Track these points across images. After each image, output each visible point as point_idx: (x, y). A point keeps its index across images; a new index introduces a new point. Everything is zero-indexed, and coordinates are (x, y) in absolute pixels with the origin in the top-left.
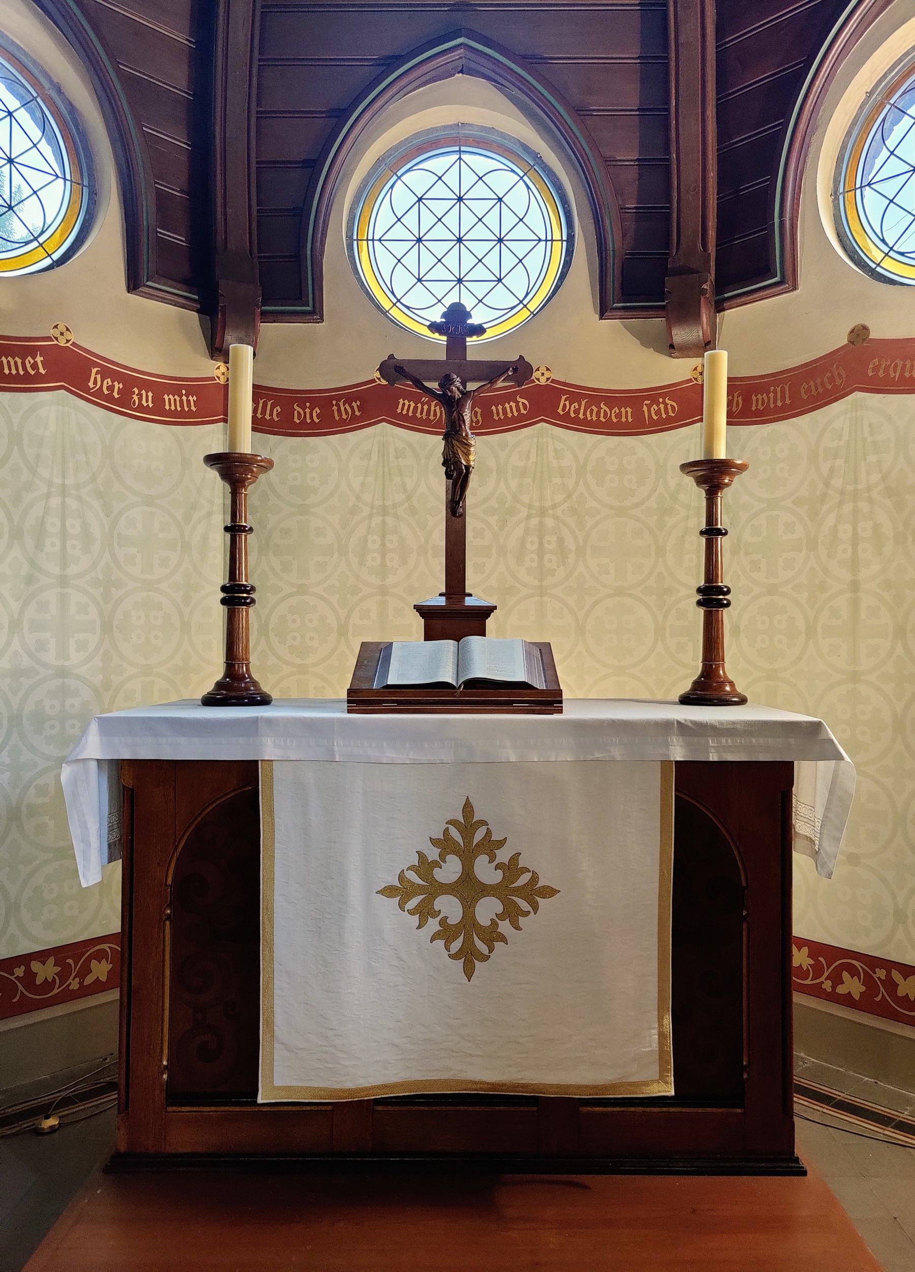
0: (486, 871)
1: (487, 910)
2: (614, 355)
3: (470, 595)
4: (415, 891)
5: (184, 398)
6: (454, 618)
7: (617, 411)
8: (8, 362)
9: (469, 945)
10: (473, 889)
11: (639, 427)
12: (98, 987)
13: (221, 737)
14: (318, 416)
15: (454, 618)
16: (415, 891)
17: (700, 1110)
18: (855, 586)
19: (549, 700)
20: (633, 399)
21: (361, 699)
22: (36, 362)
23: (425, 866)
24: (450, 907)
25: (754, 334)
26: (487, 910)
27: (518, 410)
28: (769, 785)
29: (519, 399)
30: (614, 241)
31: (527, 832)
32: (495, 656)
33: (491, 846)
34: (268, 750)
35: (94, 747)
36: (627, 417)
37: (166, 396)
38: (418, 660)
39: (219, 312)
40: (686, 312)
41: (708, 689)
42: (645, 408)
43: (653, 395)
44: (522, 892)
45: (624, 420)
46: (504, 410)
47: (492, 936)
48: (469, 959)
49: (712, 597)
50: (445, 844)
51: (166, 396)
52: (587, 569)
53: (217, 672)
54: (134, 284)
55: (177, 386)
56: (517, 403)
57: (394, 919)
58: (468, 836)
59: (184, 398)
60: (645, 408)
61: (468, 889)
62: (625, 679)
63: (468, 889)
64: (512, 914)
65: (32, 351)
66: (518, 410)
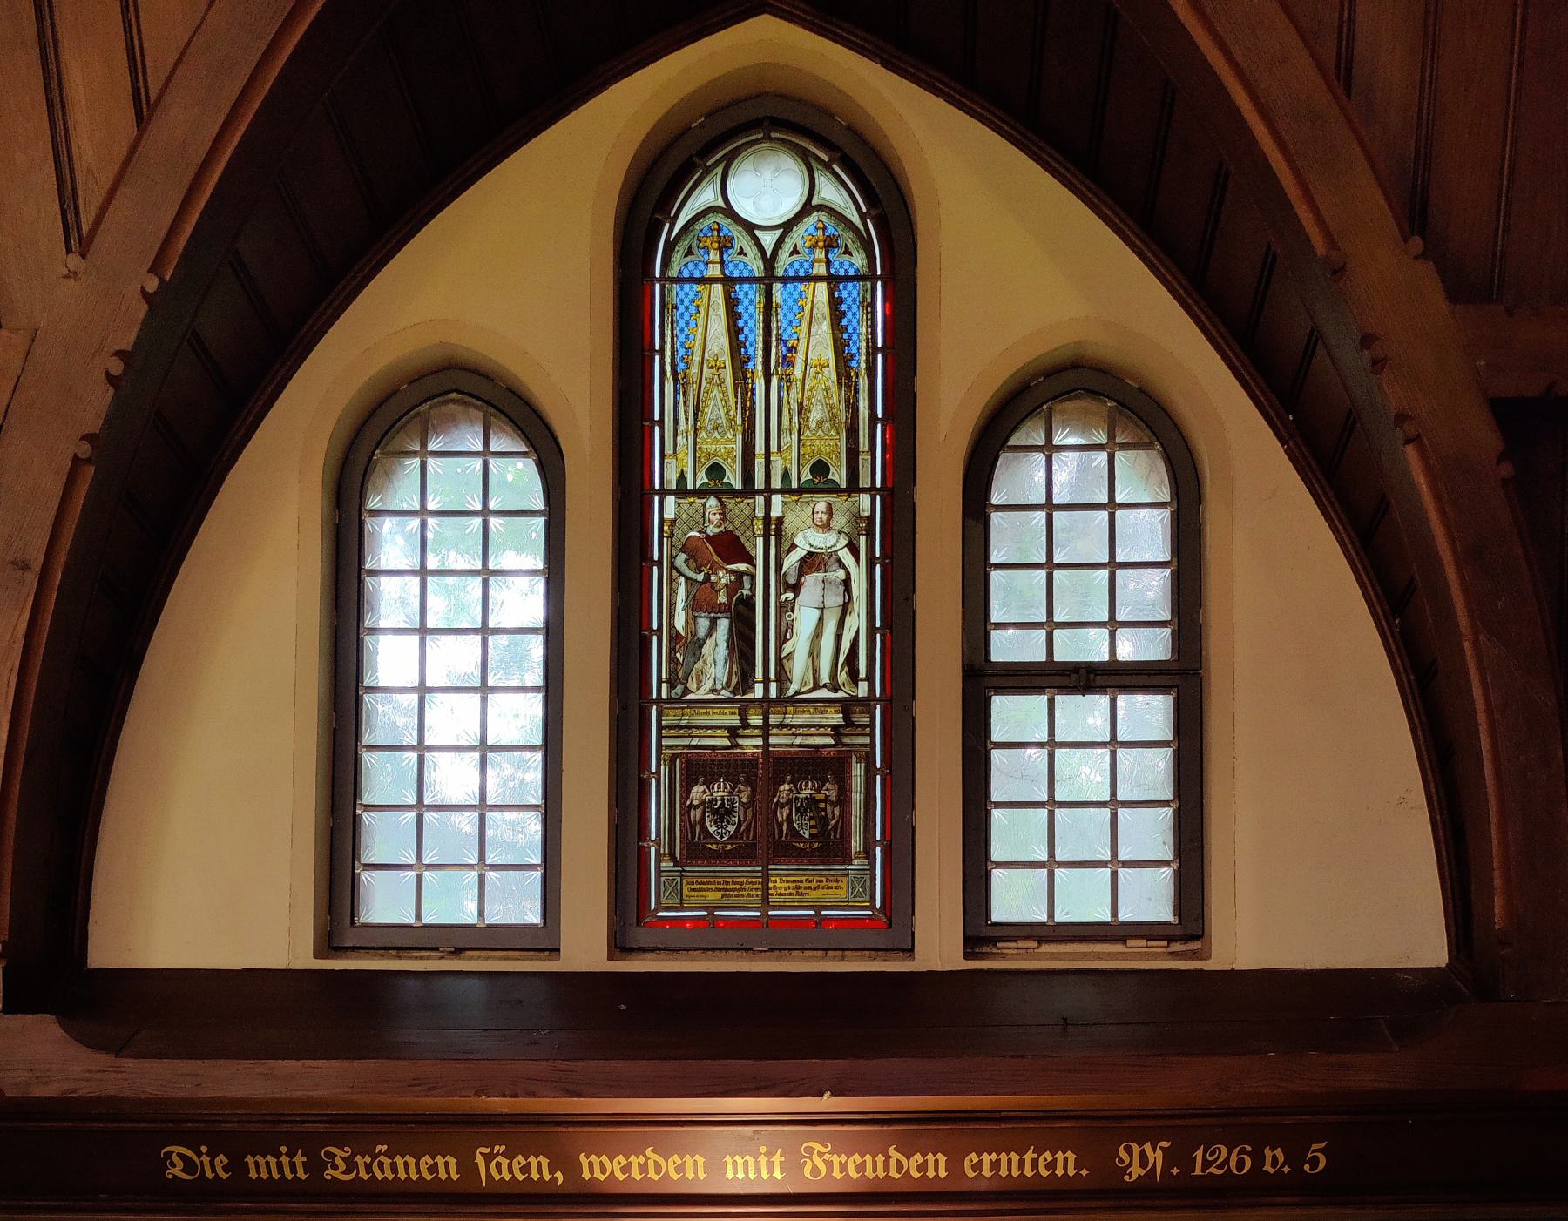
5: (285, 1160)
7: (1050, 1159)
8: (257, 1163)
14: (225, 1169)
17: (1451, 575)
19: (638, 924)
21: (890, 926)
22: (436, 1164)
27: (887, 1168)
29: (891, 1151)
36: (1065, 1168)
37: (249, 1159)
39: (820, 461)
42: (480, 1160)
45: (1060, 1172)
46: (758, 1170)
51: (249, 1159)
56: (888, 1158)
59: (285, 1160)
60: (480, 1160)
66: (887, 1168)
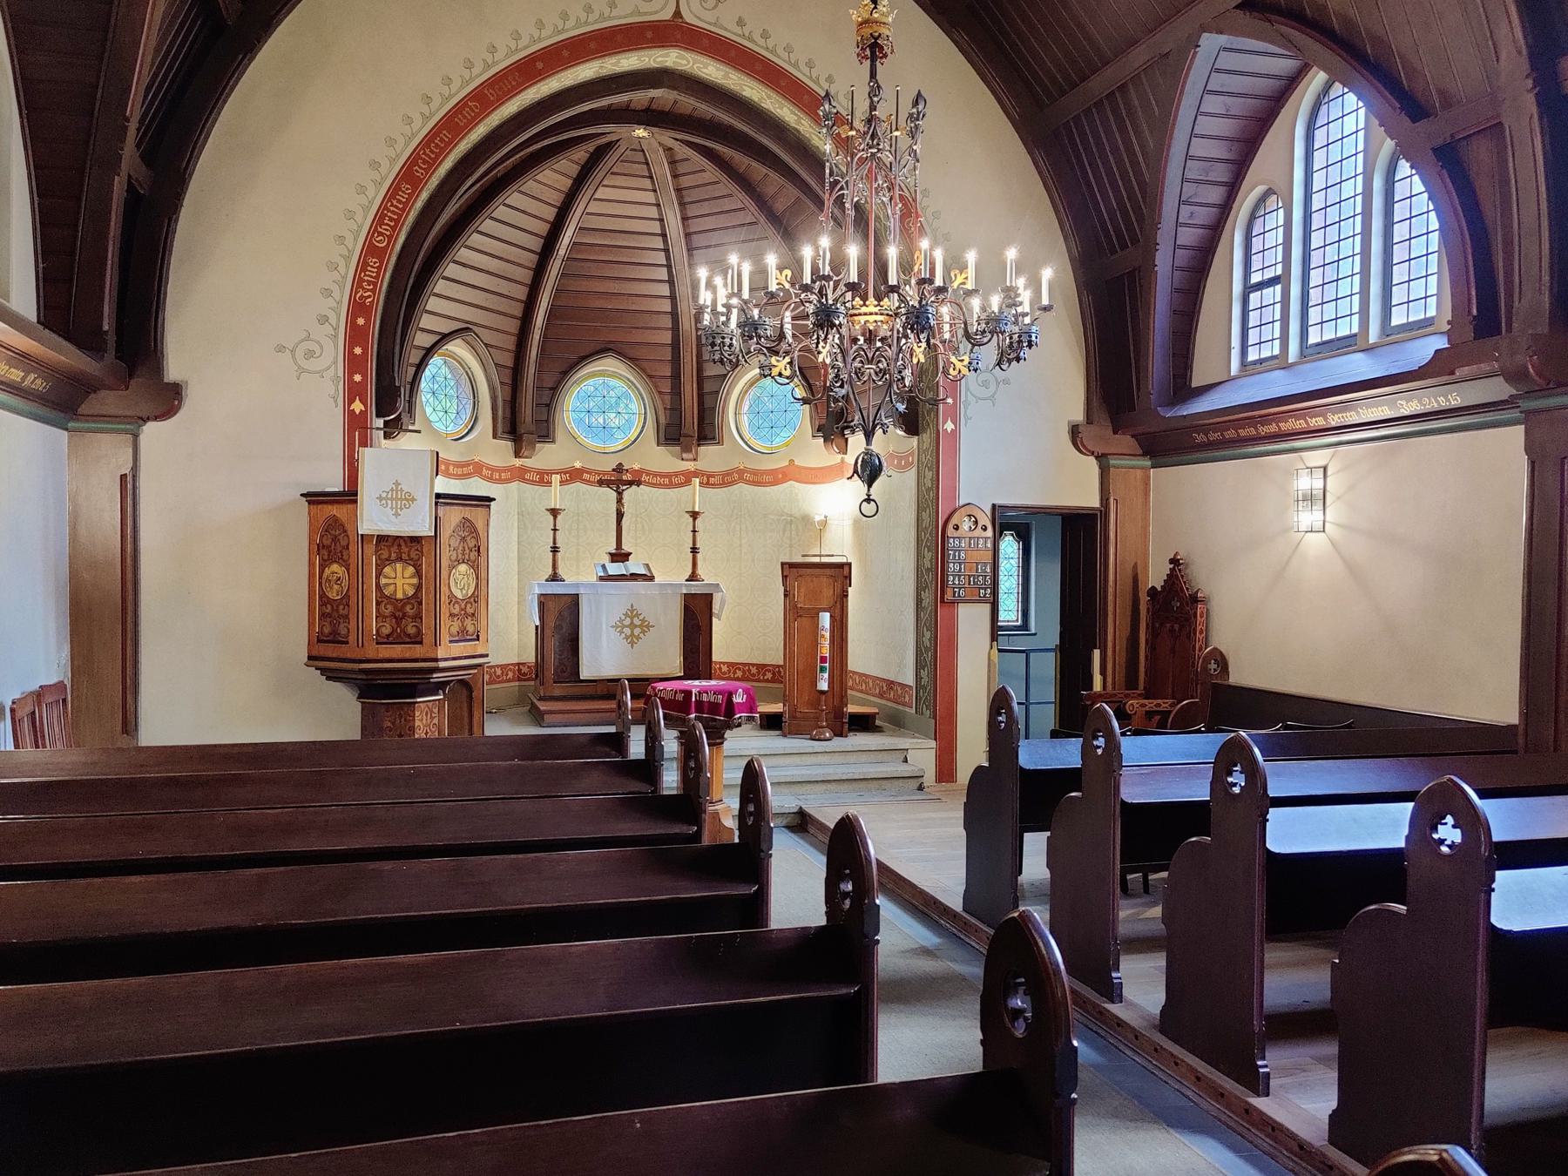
0: (637, 622)
1: (637, 631)
2: (665, 460)
3: (697, 614)
4: (619, 627)
6: (620, 556)
9: (632, 640)
10: (635, 627)
11: (671, 486)
12: (509, 681)
13: (695, 588)
15: (620, 556)
16: (619, 627)
19: (652, 578)
20: (668, 475)
23: (621, 621)
24: (627, 631)
25: (710, 457)
26: (637, 631)
28: (707, 599)
30: (663, 420)
31: (648, 612)
32: (634, 566)
33: (638, 615)
34: (581, 591)
35: (537, 591)
38: (615, 569)
40: (687, 449)
41: (693, 577)
43: (676, 474)
44: (646, 627)
47: (638, 638)
48: (632, 643)
49: (694, 550)
50: (626, 615)
52: (658, 533)
53: (550, 571)
54: (495, 437)
55: (505, 469)
57: (614, 634)
58: (632, 613)
61: (632, 626)
62: (672, 575)
63: (632, 626)
64: (643, 632)
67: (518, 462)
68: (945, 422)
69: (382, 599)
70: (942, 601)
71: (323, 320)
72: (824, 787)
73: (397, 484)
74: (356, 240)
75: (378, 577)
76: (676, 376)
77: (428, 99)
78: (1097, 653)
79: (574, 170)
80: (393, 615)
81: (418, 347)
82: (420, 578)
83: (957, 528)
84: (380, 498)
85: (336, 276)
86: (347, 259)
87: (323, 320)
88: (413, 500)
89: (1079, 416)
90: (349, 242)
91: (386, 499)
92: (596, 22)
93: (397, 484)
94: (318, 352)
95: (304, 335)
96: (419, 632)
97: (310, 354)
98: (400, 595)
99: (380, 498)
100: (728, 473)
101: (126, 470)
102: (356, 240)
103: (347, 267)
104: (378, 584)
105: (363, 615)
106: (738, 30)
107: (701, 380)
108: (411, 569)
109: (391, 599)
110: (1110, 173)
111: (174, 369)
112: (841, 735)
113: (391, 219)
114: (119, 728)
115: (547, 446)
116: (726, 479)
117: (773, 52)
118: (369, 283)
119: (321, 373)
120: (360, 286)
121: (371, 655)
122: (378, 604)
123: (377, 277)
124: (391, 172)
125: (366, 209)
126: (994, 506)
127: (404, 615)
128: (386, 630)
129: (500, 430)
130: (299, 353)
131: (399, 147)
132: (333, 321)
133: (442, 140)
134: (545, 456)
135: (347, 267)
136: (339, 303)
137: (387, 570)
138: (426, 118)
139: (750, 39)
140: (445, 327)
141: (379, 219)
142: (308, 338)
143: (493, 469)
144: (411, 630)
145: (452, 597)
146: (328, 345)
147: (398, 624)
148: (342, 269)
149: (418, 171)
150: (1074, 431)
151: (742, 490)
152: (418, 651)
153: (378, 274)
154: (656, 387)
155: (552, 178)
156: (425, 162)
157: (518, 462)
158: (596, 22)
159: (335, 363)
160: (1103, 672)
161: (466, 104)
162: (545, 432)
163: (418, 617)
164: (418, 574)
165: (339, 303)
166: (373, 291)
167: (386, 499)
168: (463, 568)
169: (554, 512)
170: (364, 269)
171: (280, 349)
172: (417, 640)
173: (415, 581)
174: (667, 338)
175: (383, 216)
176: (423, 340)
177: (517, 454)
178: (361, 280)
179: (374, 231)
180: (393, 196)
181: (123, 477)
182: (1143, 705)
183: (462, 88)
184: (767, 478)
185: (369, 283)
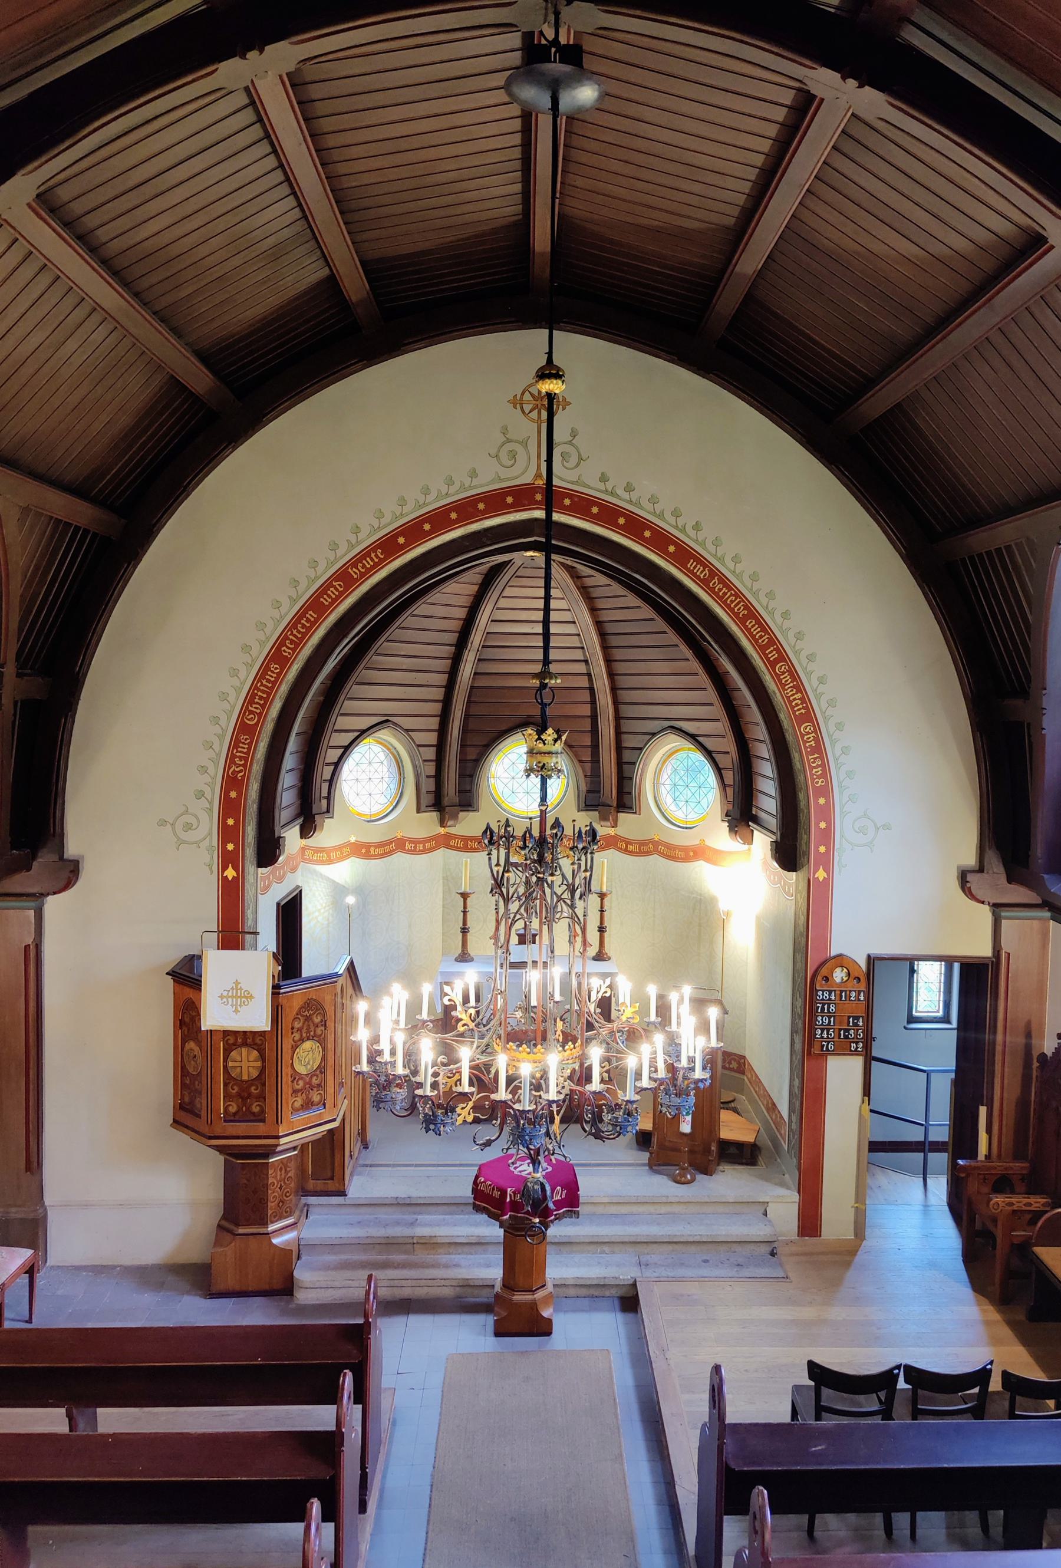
18: (654, 916)
54: (418, 811)
55: (429, 839)
65: (391, 843)
67: (442, 831)
68: (816, 870)
69: (229, 1079)
70: (809, 1053)
71: (200, 795)
72: (670, 1247)
73: (237, 983)
74: (229, 719)
75: (225, 1060)
76: (595, 746)
77: (295, 583)
78: (983, 1110)
79: (479, 579)
80: (239, 1095)
81: (328, 764)
82: (263, 1060)
83: (827, 979)
84: (221, 997)
85: (211, 754)
86: (221, 737)
87: (200, 795)
88: (251, 997)
89: (969, 858)
90: (223, 722)
91: (228, 997)
92: (457, 493)
93: (237, 983)
94: (193, 821)
95: (184, 808)
96: (262, 1111)
97: (188, 827)
98: (245, 1077)
99: (221, 997)
100: (643, 843)
101: (30, 940)
102: (229, 719)
103: (221, 745)
104: (225, 1067)
105: (212, 1096)
106: (601, 486)
107: (619, 749)
108: (255, 1053)
109: (239, 1082)
110: (1003, 615)
111: (72, 849)
112: (707, 1171)
113: (261, 698)
114: (23, 1166)
115: (471, 813)
116: (643, 848)
117: (638, 504)
118: (241, 758)
119: (197, 843)
120: (232, 762)
121: (218, 1132)
122: (226, 1085)
123: (248, 753)
124: (260, 653)
125: (238, 690)
126: (869, 956)
127: (250, 1095)
128: (233, 1109)
129: (424, 803)
130: (179, 826)
131: (268, 630)
132: (208, 796)
133: (308, 620)
134: (470, 824)
135: (221, 745)
136: (214, 778)
137: (234, 1054)
138: (294, 601)
139: (612, 494)
140: (364, 723)
141: (250, 699)
142: (186, 812)
143: (416, 842)
144: (255, 1109)
145: (295, 1076)
146: (204, 817)
147: (244, 1104)
148: (216, 747)
149: (286, 651)
150: (963, 877)
151: (655, 861)
152: (261, 1128)
153: (249, 749)
154: (576, 756)
155: (457, 592)
156: (292, 642)
157: (442, 831)
158: (457, 493)
159: (210, 834)
160: (989, 1131)
161: (286, 638)
162: (467, 801)
163: (262, 1097)
164: (262, 1057)
165: (214, 778)
166: (245, 766)
167: (228, 997)
168: (308, 1045)
169: (465, 896)
170: (236, 746)
171: (163, 823)
172: (260, 1118)
173: (259, 1064)
174: (586, 710)
175: (254, 695)
176: (333, 755)
177: (442, 824)
178: (234, 756)
179: (245, 710)
180: (263, 677)
181: (27, 947)
182: (1011, 1204)
183: (327, 569)
184: (679, 854)
185: (241, 758)
